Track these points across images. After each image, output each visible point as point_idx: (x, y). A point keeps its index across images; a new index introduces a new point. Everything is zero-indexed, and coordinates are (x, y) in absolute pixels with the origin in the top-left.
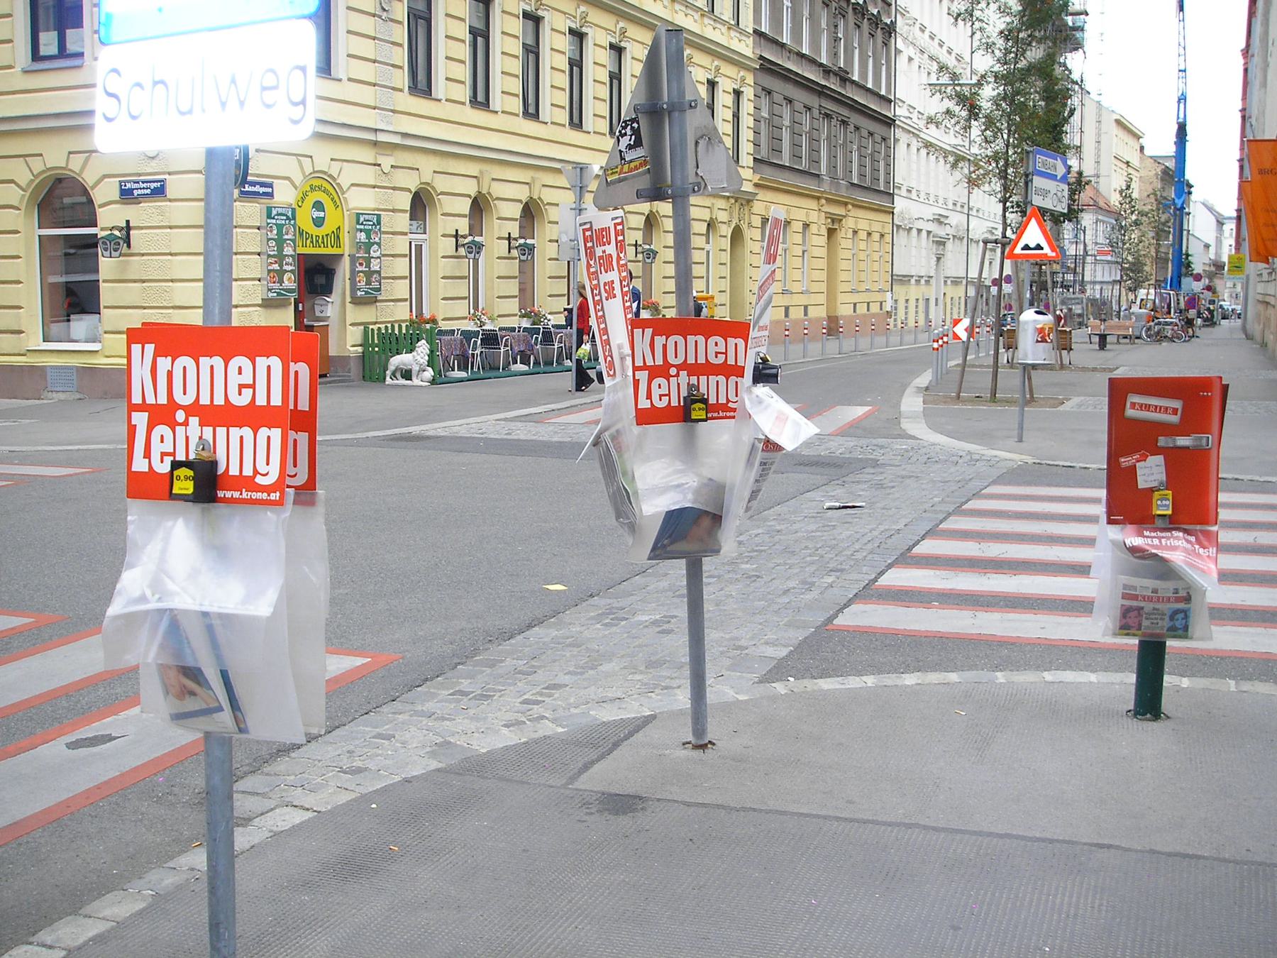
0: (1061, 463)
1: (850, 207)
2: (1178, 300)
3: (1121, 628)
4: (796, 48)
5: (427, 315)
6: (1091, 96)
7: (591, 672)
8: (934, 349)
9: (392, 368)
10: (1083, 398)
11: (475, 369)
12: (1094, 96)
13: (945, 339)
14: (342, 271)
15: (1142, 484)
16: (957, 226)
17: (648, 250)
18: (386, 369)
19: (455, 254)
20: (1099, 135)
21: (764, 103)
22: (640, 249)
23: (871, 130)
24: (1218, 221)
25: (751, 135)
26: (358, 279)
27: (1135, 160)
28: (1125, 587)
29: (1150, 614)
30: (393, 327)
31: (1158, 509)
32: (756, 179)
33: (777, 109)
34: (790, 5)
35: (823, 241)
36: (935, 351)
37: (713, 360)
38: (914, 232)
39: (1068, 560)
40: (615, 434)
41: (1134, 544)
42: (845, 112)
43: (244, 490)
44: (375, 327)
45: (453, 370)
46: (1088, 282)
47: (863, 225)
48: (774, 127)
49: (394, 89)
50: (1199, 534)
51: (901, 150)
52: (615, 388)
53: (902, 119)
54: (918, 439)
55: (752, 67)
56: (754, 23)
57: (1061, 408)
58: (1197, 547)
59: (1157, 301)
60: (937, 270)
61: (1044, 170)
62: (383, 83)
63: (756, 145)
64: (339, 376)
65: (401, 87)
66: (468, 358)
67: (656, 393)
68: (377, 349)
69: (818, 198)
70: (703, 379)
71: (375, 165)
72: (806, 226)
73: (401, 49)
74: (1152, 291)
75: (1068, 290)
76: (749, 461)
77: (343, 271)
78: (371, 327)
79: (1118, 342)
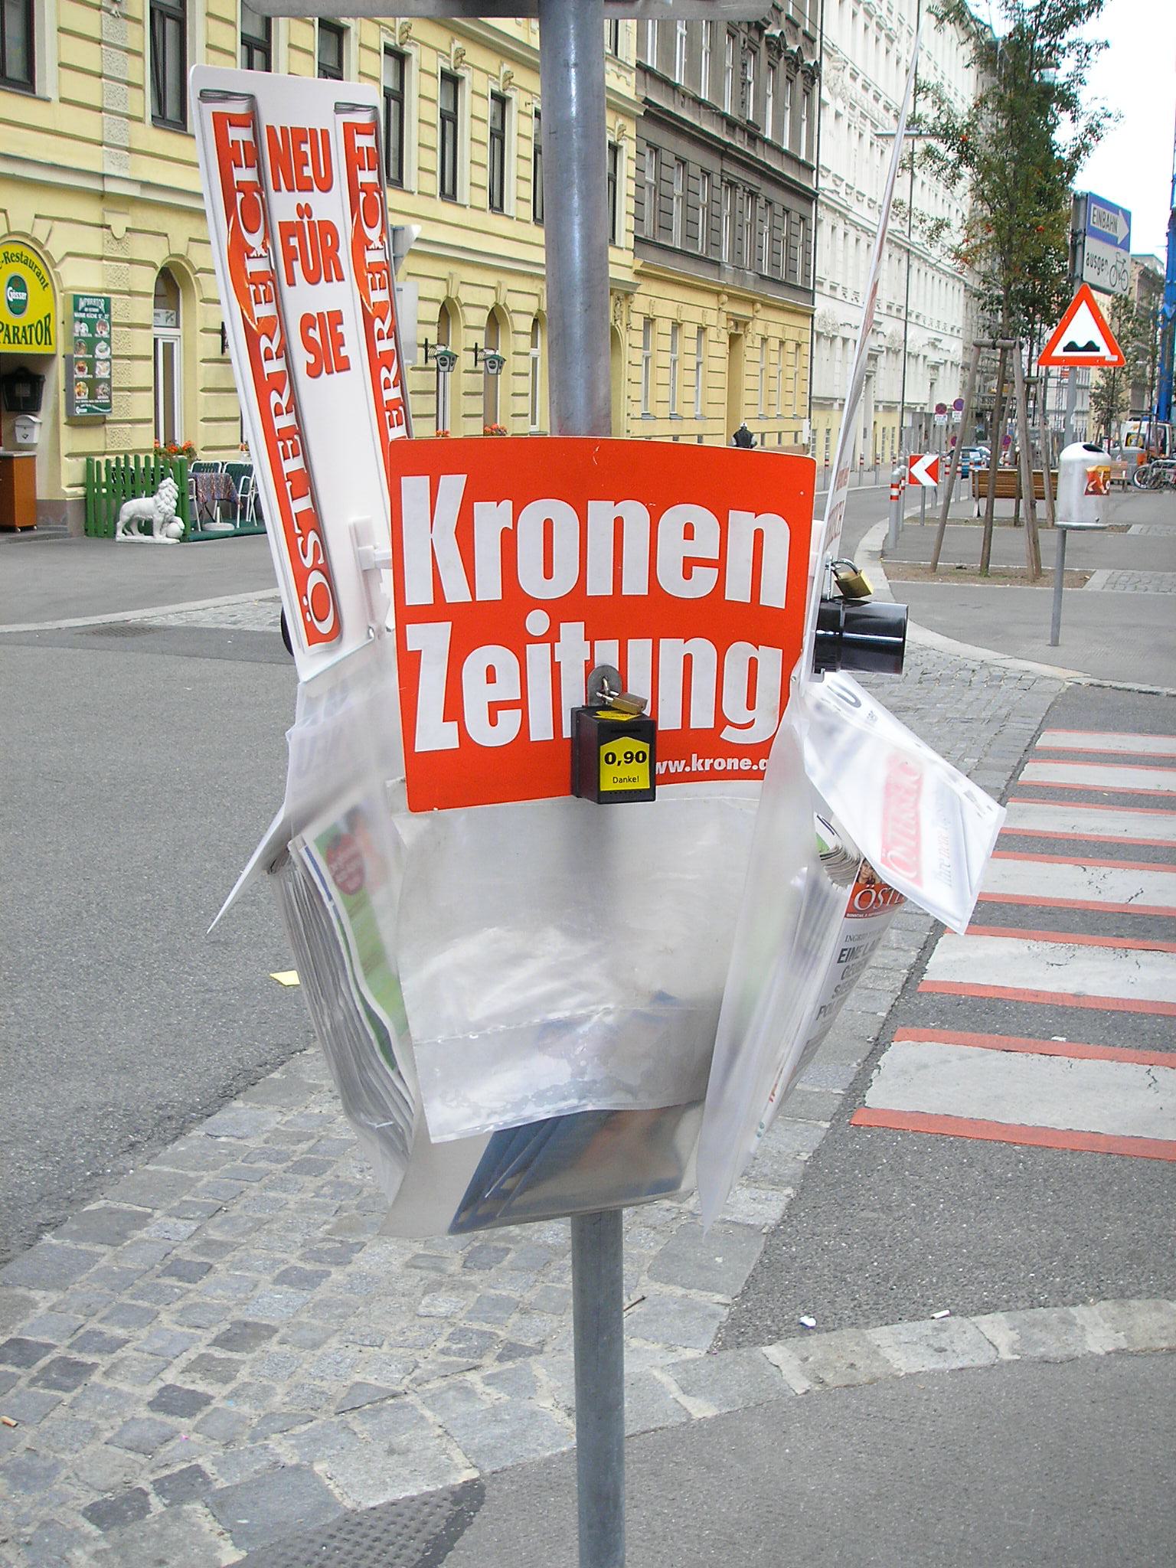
0: (1136, 686)
1: (758, 306)
4: (691, 90)
5: (180, 441)
7: (337, 1275)
8: (892, 497)
9: (124, 517)
11: (248, 519)
14: (54, 376)
16: (892, 336)
17: (492, 357)
18: (116, 519)
19: (220, 357)
21: (649, 160)
22: (480, 356)
25: (631, 206)
26: (76, 391)
30: (127, 459)
32: (638, 265)
33: (666, 173)
34: (685, 32)
35: (722, 350)
37: (674, 585)
38: (839, 342)
40: (344, 829)
42: (753, 180)
43: (694, 756)
44: (102, 459)
45: (215, 521)
46: (1051, 411)
47: (774, 331)
48: (662, 196)
49: (130, 117)
51: (824, 235)
52: (337, 681)
53: (826, 193)
55: (634, 113)
56: (637, 55)
61: (1099, 227)
62: (114, 108)
63: (639, 219)
64: (50, 529)
65: (141, 116)
66: (236, 504)
67: (476, 696)
68: (104, 491)
69: (718, 294)
70: (639, 649)
71: (102, 226)
72: (702, 330)
73: (141, 60)
76: (803, 951)
77: (56, 378)
78: (97, 459)
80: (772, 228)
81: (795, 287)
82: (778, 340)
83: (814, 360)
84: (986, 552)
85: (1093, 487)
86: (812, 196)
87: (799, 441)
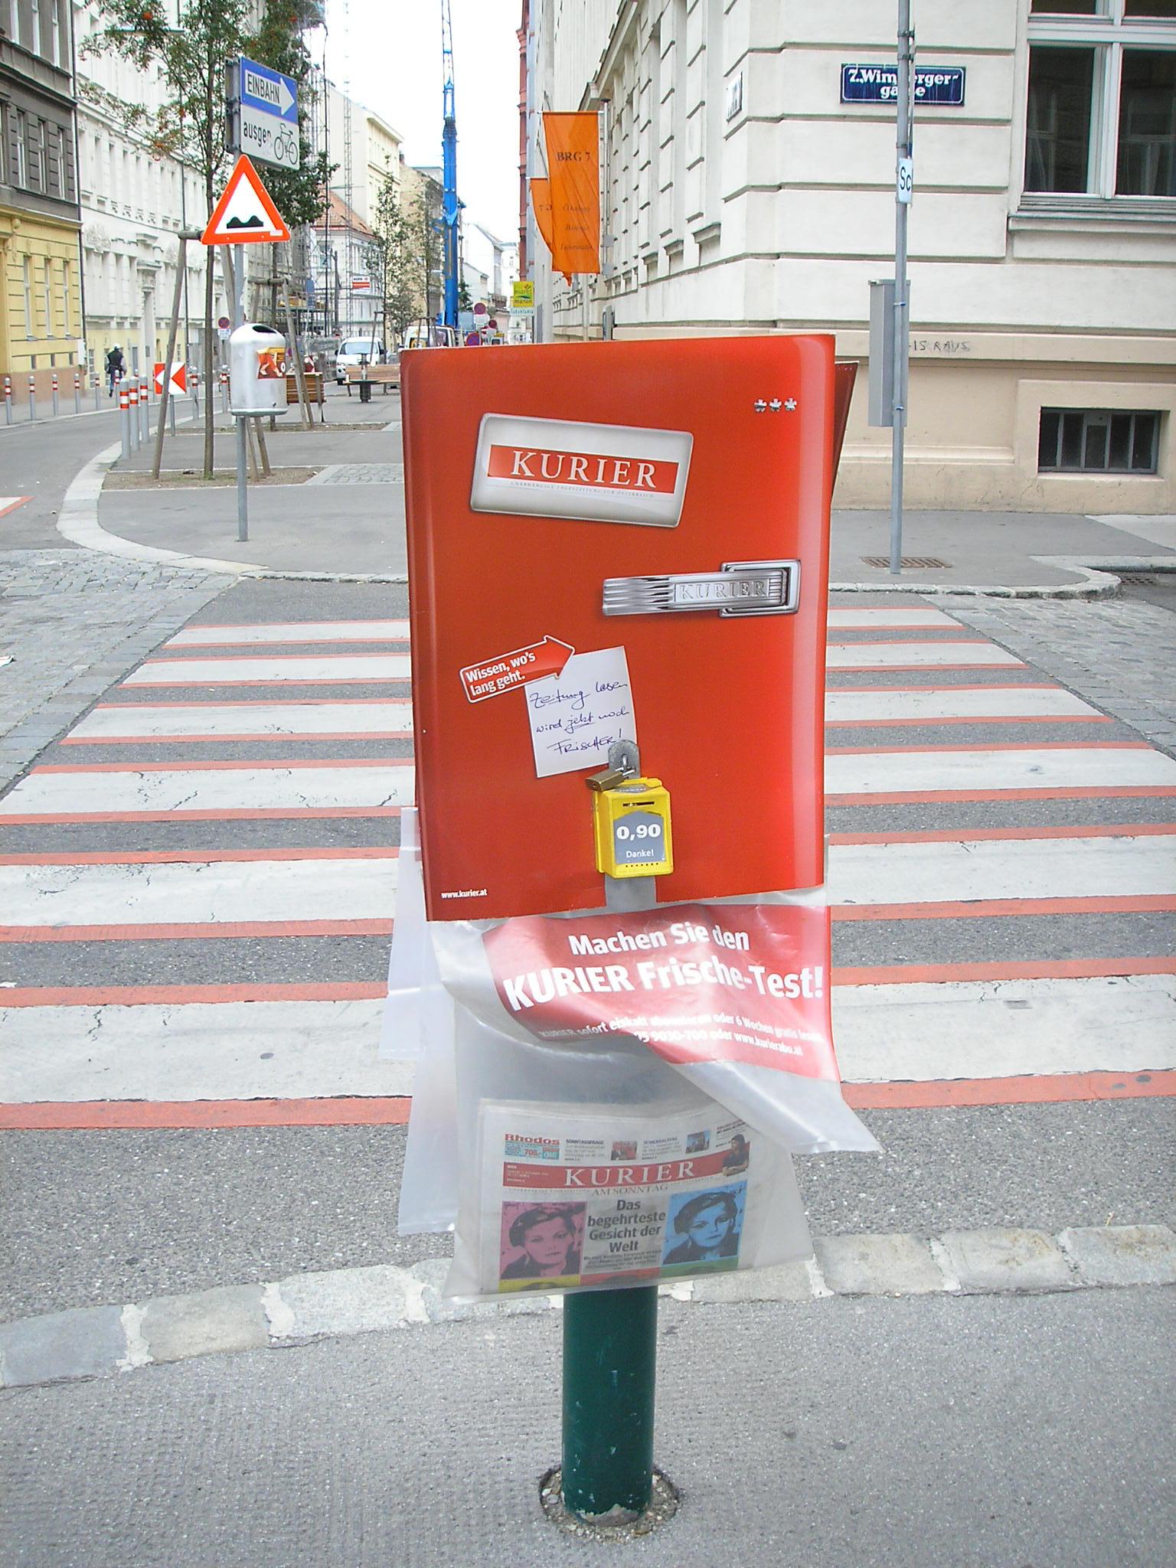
0: (309, 575)
1: (17, 222)
2: (456, 339)
3: (510, 1272)
6: (336, 89)
10: (342, 466)
12: (340, 87)
13: (144, 392)
15: (549, 762)
16: (170, 251)
20: (348, 133)
23: (43, 115)
24: (495, 247)
27: (394, 168)
28: (513, 1143)
29: (607, 1222)
31: (622, 860)
36: (124, 410)
38: (111, 258)
39: (324, 804)
41: (541, 999)
47: (37, 248)
50: (762, 920)
51: (86, 147)
54: (82, 547)
57: (309, 483)
58: (758, 970)
59: (431, 340)
60: (145, 308)
74: (425, 328)
75: (319, 333)
79: (385, 393)
80: (27, 139)
81: (59, 202)
82: (43, 257)
83: (85, 278)
84: (208, 454)
85: (266, 370)
86: (69, 105)
87: (74, 362)
